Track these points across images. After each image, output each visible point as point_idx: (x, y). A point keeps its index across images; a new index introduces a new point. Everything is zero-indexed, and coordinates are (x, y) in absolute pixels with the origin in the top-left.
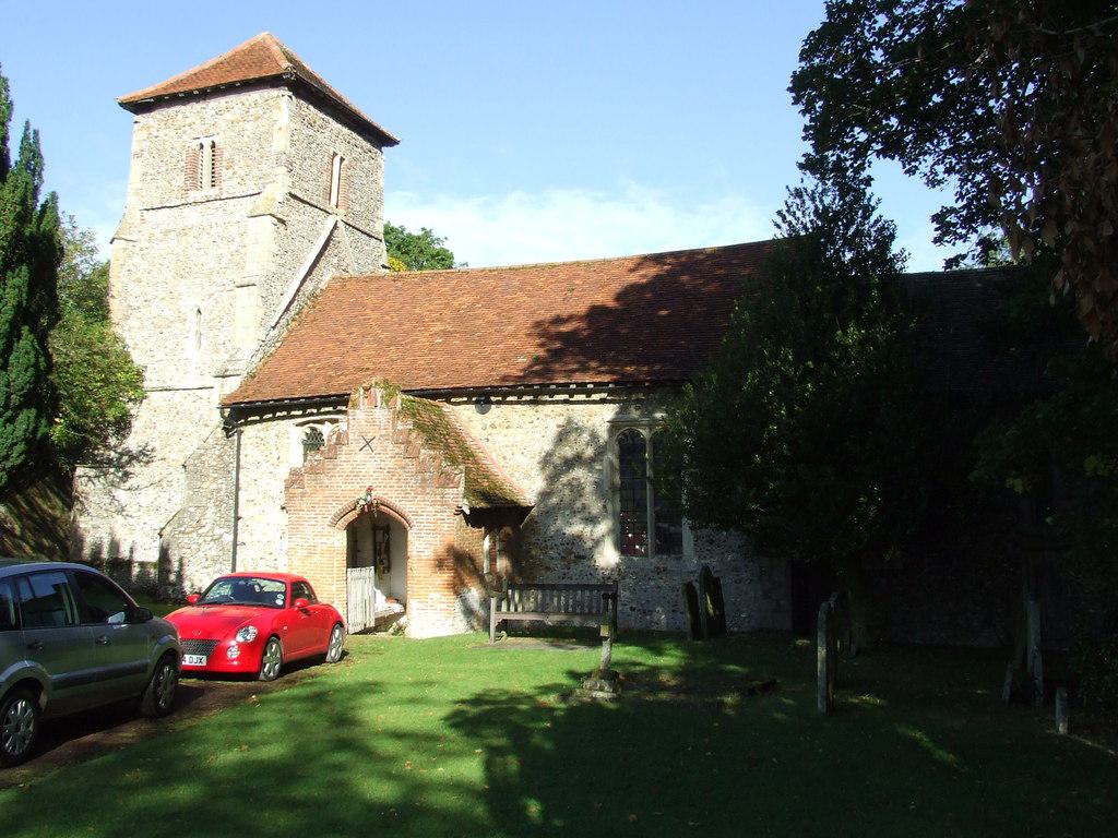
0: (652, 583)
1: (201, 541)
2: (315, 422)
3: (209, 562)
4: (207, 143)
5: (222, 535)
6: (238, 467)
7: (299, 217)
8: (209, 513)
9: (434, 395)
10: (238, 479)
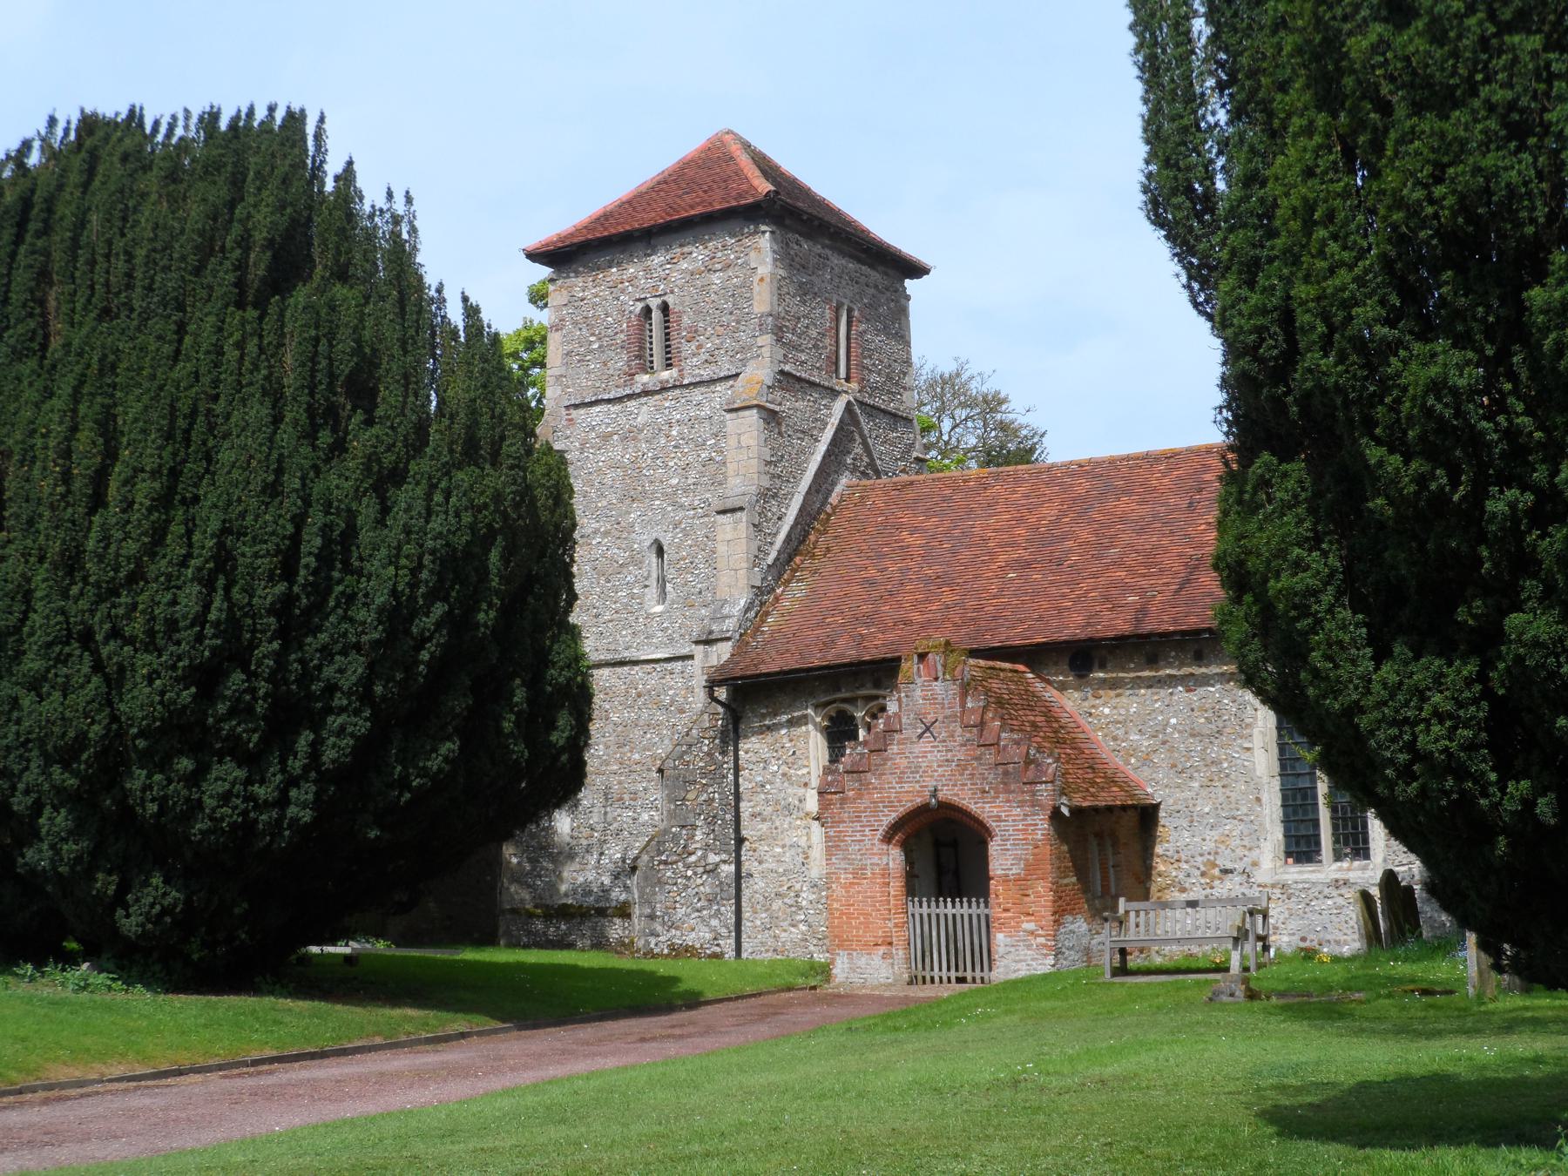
0: (1330, 902)
1: (690, 873)
2: (844, 700)
4: (654, 303)
5: (717, 865)
6: (737, 769)
7: (794, 406)
8: (699, 836)
9: (1036, 656)
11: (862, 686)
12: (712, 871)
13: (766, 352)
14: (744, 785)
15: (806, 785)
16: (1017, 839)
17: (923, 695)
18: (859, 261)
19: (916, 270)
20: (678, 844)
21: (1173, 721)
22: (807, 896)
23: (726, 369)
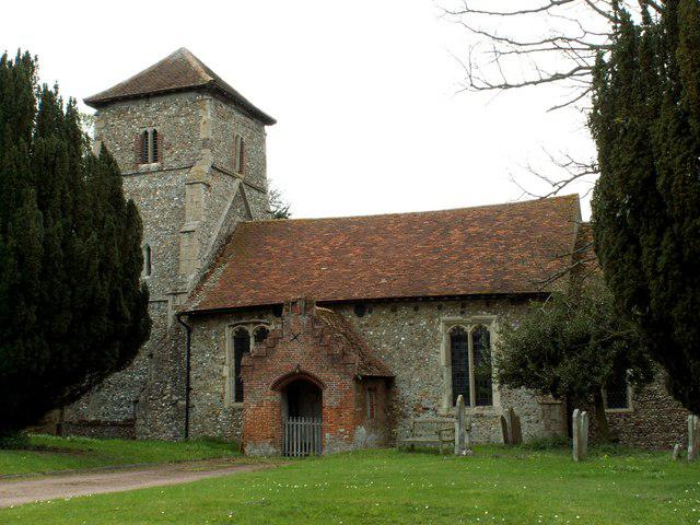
4: (150, 130)
6: (189, 355)
10: (189, 363)
14: (192, 363)
19: (269, 121)
23: (185, 162)
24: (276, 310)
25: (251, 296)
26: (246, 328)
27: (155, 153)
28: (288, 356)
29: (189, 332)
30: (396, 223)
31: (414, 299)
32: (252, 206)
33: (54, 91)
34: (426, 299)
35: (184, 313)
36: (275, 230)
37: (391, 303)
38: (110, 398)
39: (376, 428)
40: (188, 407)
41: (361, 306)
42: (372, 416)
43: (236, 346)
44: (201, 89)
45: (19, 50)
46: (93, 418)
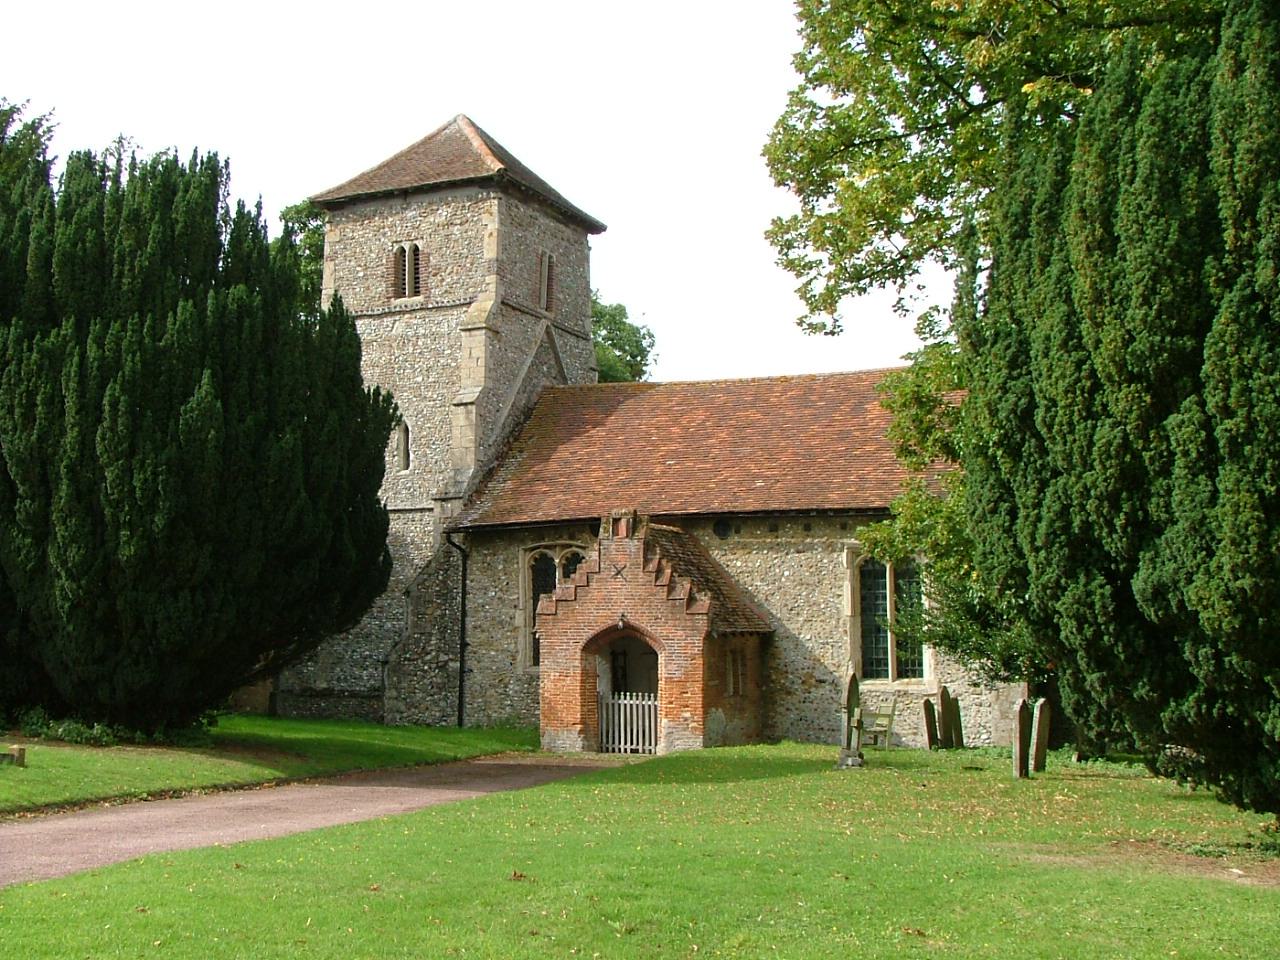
2: (546, 547)
3: (435, 690)
6: (465, 593)
9: (691, 521)
10: (464, 605)
11: (561, 537)
12: (443, 667)
13: (492, 287)
14: (469, 605)
15: (515, 607)
16: (679, 654)
17: (619, 549)
18: (558, 221)
19: (596, 228)
20: (418, 647)
21: (786, 573)
22: (512, 688)
23: (460, 295)
24: (592, 526)
25: (557, 504)
26: (549, 553)
27: (416, 280)
28: (607, 600)
29: (466, 557)
30: (784, 392)
31: (805, 513)
32: (566, 360)
33: (254, 212)
34: (822, 513)
35: (457, 530)
36: (597, 402)
37: (771, 521)
38: (349, 659)
39: (742, 710)
40: (463, 672)
41: (725, 523)
42: (736, 692)
43: (534, 580)
44: (485, 183)
45: (195, 151)
46: (324, 685)
